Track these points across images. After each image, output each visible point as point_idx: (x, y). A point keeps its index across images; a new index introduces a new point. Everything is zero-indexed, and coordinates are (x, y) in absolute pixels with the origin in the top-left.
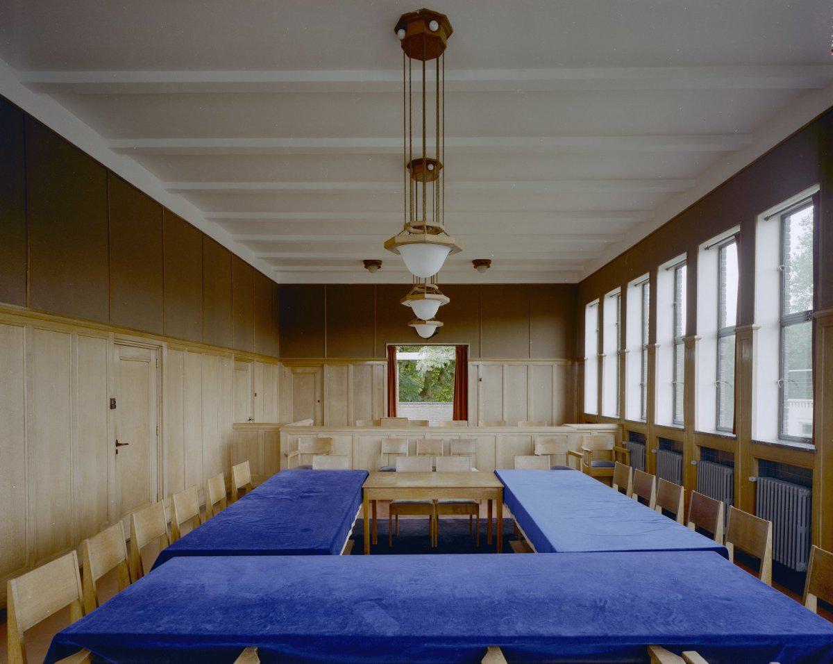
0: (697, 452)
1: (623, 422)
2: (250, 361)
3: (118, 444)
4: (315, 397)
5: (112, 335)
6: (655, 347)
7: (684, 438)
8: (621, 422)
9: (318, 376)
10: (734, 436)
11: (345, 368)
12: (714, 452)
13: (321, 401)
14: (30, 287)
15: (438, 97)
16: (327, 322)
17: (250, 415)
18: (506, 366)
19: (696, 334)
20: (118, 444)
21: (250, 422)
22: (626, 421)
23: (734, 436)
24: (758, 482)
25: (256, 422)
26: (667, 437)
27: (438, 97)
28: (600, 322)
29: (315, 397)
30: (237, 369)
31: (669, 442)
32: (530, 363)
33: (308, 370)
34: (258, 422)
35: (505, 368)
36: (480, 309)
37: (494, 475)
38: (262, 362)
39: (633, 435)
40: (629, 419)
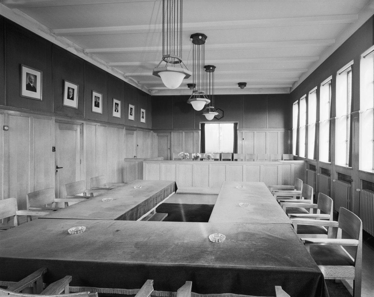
0: (336, 176)
1: (307, 160)
2: (135, 130)
3: (57, 168)
4: (167, 147)
5: (54, 118)
6: (319, 123)
7: (329, 168)
8: (306, 160)
9: (169, 138)
10: (330, 163)
11: (192, 134)
12: (343, 177)
13: (170, 149)
14: (85, 104)
15: (163, 35)
16: (169, 114)
17: (135, 155)
18: (255, 132)
19: (335, 116)
20: (57, 168)
21: (135, 158)
22: (308, 159)
23: (330, 163)
24: (361, 192)
25: (138, 158)
26: (325, 167)
27: (163, 35)
28: (301, 111)
29: (167, 147)
30: (127, 134)
31: (325, 171)
32: (267, 131)
33: (166, 134)
34: (139, 158)
35: (255, 134)
36: (238, 107)
37: (62, 167)
38: (141, 131)
39: (311, 166)
40: (233, 151)
